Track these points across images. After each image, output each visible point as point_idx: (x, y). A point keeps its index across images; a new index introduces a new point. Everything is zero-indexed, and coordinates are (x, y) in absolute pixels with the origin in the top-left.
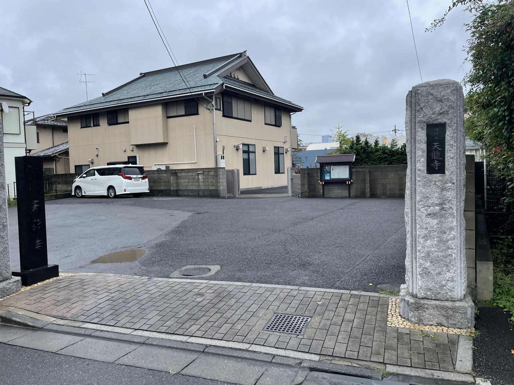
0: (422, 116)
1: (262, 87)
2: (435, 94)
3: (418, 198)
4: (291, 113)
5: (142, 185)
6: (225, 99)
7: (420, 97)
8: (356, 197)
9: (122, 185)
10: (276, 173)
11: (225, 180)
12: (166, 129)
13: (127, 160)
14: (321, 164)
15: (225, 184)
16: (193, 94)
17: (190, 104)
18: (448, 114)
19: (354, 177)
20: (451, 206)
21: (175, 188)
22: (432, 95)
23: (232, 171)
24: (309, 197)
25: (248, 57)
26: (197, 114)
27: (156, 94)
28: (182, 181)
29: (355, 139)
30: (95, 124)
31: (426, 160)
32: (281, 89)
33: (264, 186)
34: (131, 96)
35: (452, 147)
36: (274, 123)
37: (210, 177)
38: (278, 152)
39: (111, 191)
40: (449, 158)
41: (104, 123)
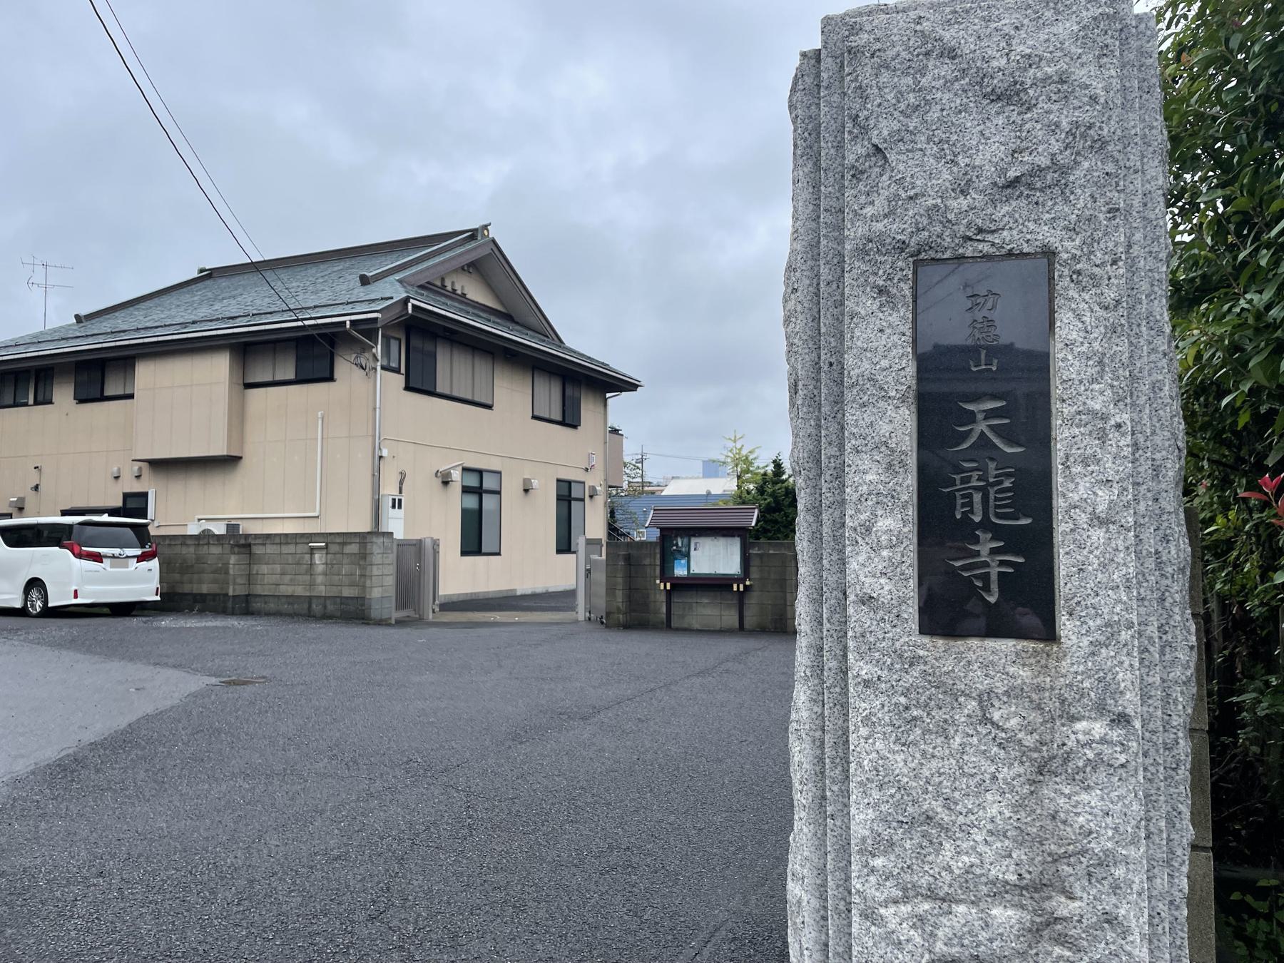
0: (880, 204)
1: (532, 320)
2: (968, 47)
3: (862, 821)
4: (608, 395)
5: (139, 580)
6: (416, 342)
7: (866, 74)
8: (761, 630)
9: (70, 577)
10: (559, 551)
11: (391, 570)
12: (238, 418)
13: (119, 503)
14: (662, 529)
15: (390, 581)
16: (307, 323)
17: (313, 352)
18: (1064, 190)
19: (755, 573)
20: (1108, 903)
21: (240, 591)
22: (951, 54)
23: (418, 545)
24: (627, 626)
25: (494, 241)
26: (330, 378)
27: (218, 319)
28: (264, 569)
29: (771, 468)
30: (40, 398)
31: (911, 530)
32: (582, 332)
33: (524, 585)
34: (148, 324)
35: (1103, 437)
36: (558, 418)
37: (346, 561)
38: (567, 496)
39: (34, 594)
40: (1083, 518)
41: (63, 394)
